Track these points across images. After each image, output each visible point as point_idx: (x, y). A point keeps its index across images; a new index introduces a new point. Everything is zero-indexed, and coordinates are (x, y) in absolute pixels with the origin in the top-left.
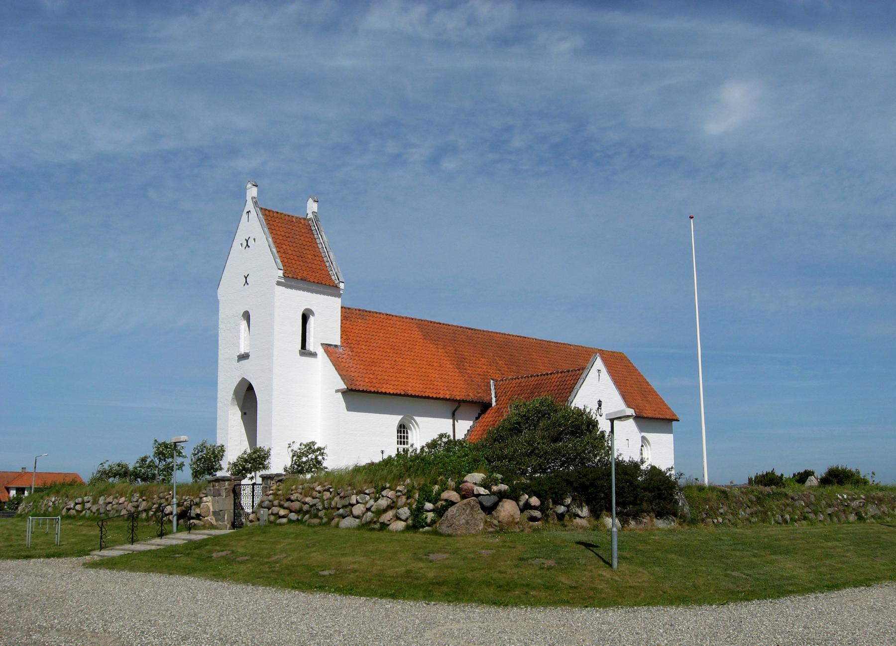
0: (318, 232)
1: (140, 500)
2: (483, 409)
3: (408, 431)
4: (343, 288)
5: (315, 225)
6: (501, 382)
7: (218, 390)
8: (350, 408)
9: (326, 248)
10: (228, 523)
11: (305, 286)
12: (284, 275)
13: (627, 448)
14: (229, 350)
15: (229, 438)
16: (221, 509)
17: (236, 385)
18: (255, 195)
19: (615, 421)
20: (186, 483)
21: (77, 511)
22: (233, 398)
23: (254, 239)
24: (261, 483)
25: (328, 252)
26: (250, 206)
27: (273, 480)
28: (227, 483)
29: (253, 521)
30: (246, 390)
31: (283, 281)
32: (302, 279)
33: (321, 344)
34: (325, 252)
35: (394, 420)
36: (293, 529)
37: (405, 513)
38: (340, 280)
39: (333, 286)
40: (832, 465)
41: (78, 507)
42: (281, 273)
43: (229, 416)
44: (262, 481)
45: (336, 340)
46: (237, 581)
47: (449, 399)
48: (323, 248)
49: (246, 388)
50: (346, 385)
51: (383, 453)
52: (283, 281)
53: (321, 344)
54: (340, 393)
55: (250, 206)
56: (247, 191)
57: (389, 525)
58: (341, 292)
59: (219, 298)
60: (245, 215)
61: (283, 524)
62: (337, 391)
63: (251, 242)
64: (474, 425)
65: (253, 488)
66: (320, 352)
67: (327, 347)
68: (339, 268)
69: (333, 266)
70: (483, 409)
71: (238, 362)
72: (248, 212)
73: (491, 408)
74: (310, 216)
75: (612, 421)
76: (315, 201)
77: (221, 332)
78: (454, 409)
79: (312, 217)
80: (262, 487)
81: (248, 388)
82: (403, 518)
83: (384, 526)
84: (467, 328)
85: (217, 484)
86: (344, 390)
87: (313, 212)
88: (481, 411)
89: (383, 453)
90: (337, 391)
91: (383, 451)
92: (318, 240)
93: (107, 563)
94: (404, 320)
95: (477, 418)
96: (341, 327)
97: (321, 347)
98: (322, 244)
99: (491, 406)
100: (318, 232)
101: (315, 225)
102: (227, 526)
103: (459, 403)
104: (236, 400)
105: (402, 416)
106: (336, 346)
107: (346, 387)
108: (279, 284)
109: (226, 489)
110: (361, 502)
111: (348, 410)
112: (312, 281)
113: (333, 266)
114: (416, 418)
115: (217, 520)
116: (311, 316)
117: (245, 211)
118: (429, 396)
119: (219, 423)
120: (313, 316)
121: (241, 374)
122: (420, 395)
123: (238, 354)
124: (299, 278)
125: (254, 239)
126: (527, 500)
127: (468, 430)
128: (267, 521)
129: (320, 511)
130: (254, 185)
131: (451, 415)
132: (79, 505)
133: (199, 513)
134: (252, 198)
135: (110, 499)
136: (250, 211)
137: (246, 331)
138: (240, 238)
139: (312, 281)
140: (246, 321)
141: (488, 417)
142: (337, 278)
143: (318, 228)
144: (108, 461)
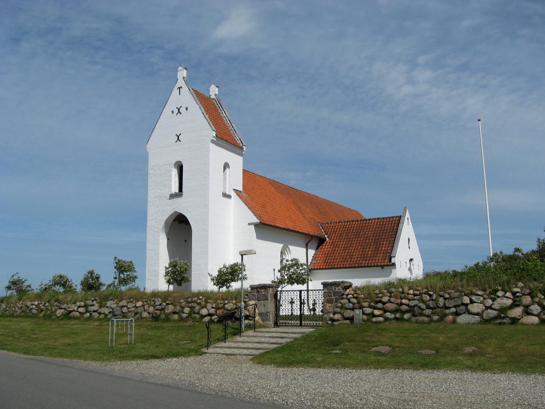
0: (221, 108)
1: (164, 304)
2: (319, 242)
3: (283, 255)
4: (245, 150)
6: (327, 225)
7: (148, 220)
8: (259, 237)
9: (229, 120)
10: (272, 323)
12: (216, 135)
13: (418, 271)
19: (244, 256)
20: (362, 286)
21: (80, 313)
23: (187, 109)
24: (322, 289)
25: (231, 123)
26: (181, 82)
28: (271, 289)
29: (340, 320)
30: (172, 221)
31: (215, 139)
33: (233, 189)
34: (228, 123)
35: (280, 246)
37: (537, 310)
38: (244, 144)
40: (155, 288)
41: (81, 310)
42: (214, 134)
44: (323, 288)
45: (240, 188)
46: (378, 365)
47: (307, 234)
48: (226, 120)
49: (173, 220)
50: (259, 220)
51: (274, 271)
53: (233, 189)
54: (253, 226)
55: (181, 82)
56: (178, 72)
57: (519, 319)
58: (244, 153)
59: (148, 151)
60: (176, 91)
64: (315, 253)
65: (308, 293)
66: (233, 194)
67: (236, 191)
69: (236, 133)
70: (319, 242)
71: (170, 199)
72: (179, 88)
73: (325, 242)
74: (213, 96)
75: (242, 255)
76: (217, 87)
80: (324, 292)
81: (174, 220)
82: (535, 313)
83: (514, 321)
84: (292, 188)
86: (259, 223)
87: (215, 95)
88: (319, 243)
89: (274, 271)
91: (274, 269)
92: (222, 114)
93: (156, 357)
95: (317, 249)
97: (233, 191)
98: (225, 117)
99: (326, 240)
100: (221, 108)
102: (272, 325)
103: (312, 237)
106: (240, 191)
107: (259, 221)
108: (212, 141)
110: (477, 301)
111: (257, 239)
113: (236, 133)
114: (290, 247)
115: (263, 320)
116: (227, 168)
117: (177, 86)
118: (298, 231)
120: (228, 169)
121: (173, 208)
122: (301, 232)
123: (170, 193)
125: (187, 109)
126: (401, 302)
127: (313, 257)
130: (185, 68)
131: (305, 245)
132: (81, 308)
134: (183, 78)
135: (123, 303)
136: (181, 87)
137: (176, 176)
138: (171, 105)
139: (230, 142)
140: (176, 169)
143: (221, 106)
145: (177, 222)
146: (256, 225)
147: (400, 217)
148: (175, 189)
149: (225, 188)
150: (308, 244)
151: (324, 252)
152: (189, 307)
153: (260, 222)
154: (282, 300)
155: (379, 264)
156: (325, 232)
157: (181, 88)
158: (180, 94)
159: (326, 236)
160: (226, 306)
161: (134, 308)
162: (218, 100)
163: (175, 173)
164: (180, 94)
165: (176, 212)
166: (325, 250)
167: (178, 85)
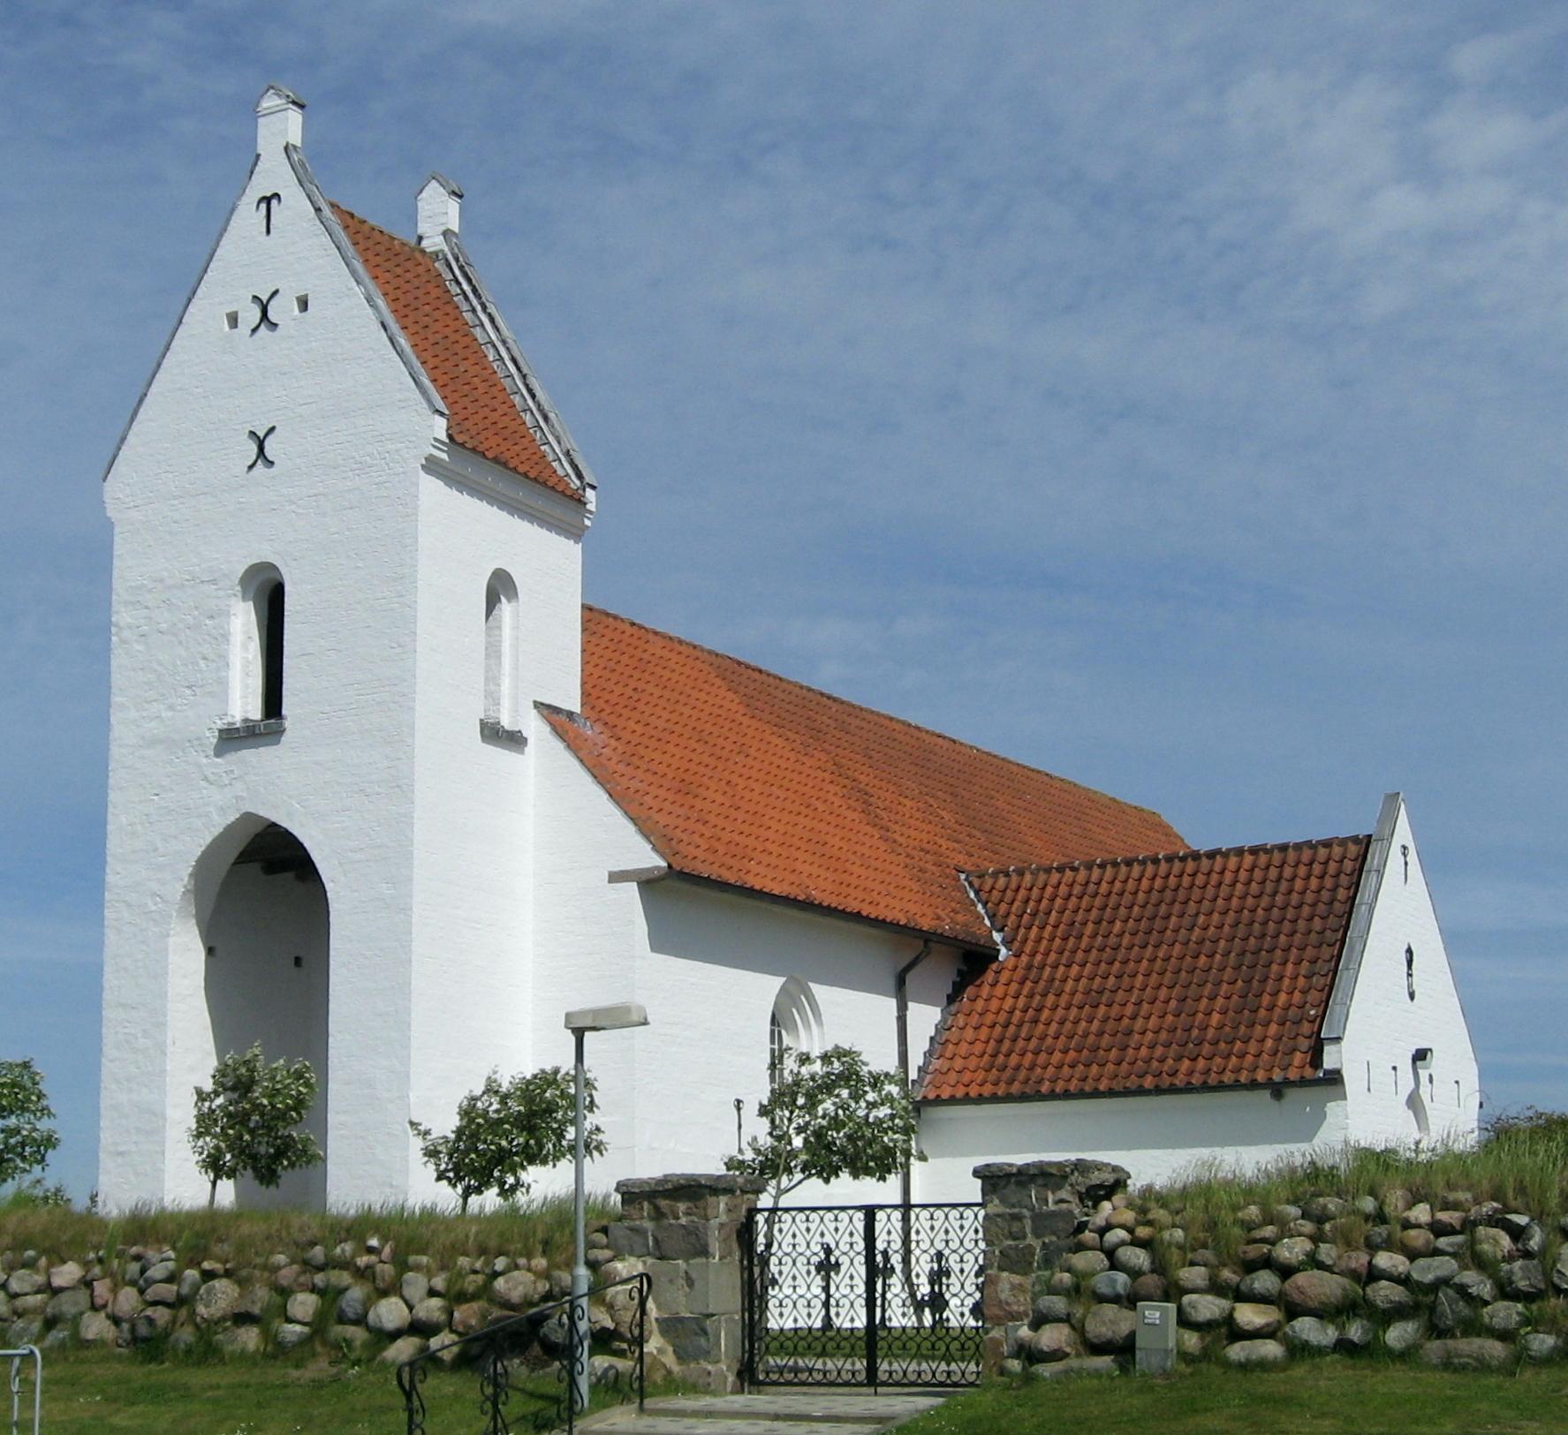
0: (475, 302)
1: (192, 1274)
3: (783, 1032)
5: (461, 279)
11: (500, 486)
12: (450, 437)
14: (171, 708)
15: (169, 1042)
16: (710, 1311)
17: (209, 839)
18: (296, 138)
22: (188, 891)
23: (304, 304)
25: (524, 377)
26: (274, 173)
27: (1059, 1187)
29: (1067, 1355)
30: (232, 860)
31: (444, 456)
32: (496, 460)
33: (535, 702)
34: (511, 376)
36: (1337, 1377)
39: (563, 492)
42: (440, 427)
43: (171, 957)
48: (501, 359)
49: (236, 854)
50: (663, 856)
51: (739, 1109)
52: (444, 456)
53: (535, 702)
55: (274, 173)
56: (261, 120)
58: (587, 522)
60: (248, 216)
61: (1263, 1365)
62: (616, 877)
63: (252, 315)
64: (944, 1020)
65: (906, 1219)
66: (534, 728)
67: (548, 711)
68: (572, 441)
70: (965, 968)
72: (267, 200)
73: (994, 966)
74: (433, 243)
77: (124, 641)
78: (903, 964)
79: (446, 249)
80: (986, 1217)
85: (682, 1207)
87: (446, 234)
88: (960, 973)
89: (739, 1109)
90: (616, 877)
94: (676, 645)
95: (951, 999)
96: (583, 651)
100: (475, 302)
101: (461, 279)
102: (726, 1378)
103: (926, 942)
104: (196, 896)
105: (811, 985)
106: (570, 714)
109: (722, 1225)
112: (521, 469)
114: (816, 988)
115: (681, 1356)
116: (503, 599)
119: (114, 984)
120: (509, 601)
123: (220, 724)
124: (490, 455)
125: (304, 304)
127: (932, 1039)
128: (1175, 1351)
129: (1486, 1303)
130: (294, 103)
131: (891, 983)
133: (610, 1325)
134: (286, 149)
136: (277, 196)
139: (521, 469)
140: (251, 603)
141: (992, 993)
142: (570, 471)
143: (475, 291)
144: (1421, 1056)
145: (254, 869)
146: (649, 884)
147: (1365, 844)
148: (246, 703)
149: (493, 698)
150: (909, 977)
151: (989, 1018)
152: (313, 1289)
153: (670, 866)
154: (780, 1254)
155: (1260, 1076)
156: (992, 917)
157: (274, 202)
158: (268, 232)
159: (997, 937)
160: (500, 1284)
161: (39, 1297)
162: (457, 260)
163: (244, 622)
164: (268, 232)
165: (248, 817)
166: (994, 1004)
167: (259, 187)
